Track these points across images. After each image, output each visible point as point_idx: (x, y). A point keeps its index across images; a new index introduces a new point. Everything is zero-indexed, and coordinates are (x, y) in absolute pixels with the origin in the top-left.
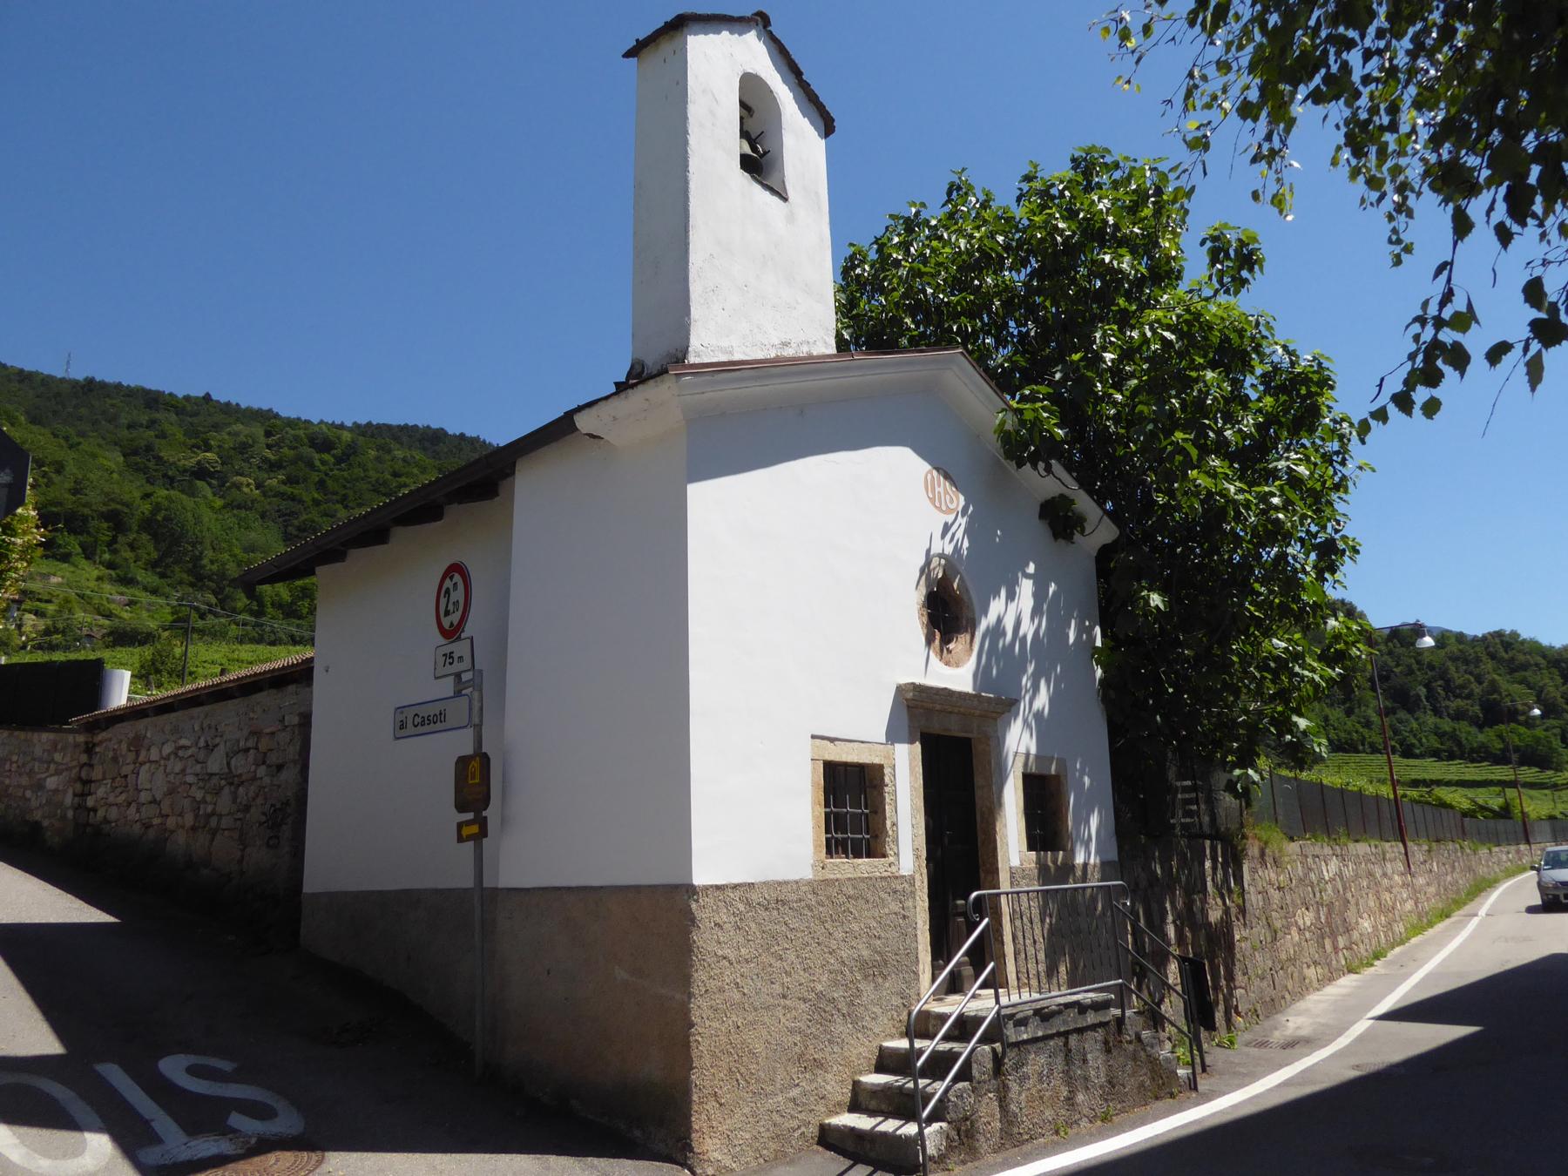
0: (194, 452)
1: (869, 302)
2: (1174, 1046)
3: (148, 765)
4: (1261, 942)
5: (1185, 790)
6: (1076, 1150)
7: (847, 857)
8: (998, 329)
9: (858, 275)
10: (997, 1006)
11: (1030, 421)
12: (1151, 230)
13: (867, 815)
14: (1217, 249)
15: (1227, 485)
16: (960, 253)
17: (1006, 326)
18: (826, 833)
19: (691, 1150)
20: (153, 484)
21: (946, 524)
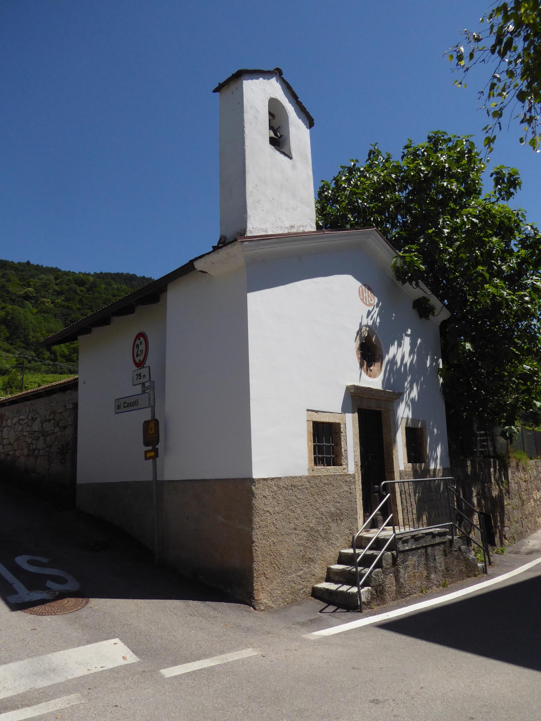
0: (23, 288)
1: (331, 208)
2: (476, 553)
3: (6, 428)
4: (517, 506)
5: (481, 435)
6: (431, 600)
7: (324, 466)
8: (392, 219)
9: (326, 195)
10: (394, 534)
11: (408, 261)
12: (466, 170)
13: (333, 446)
14: (499, 178)
15: (503, 292)
16: (374, 183)
17: (396, 218)
18: (314, 454)
19: (254, 599)
20: (5, 303)
21: (369, 311)
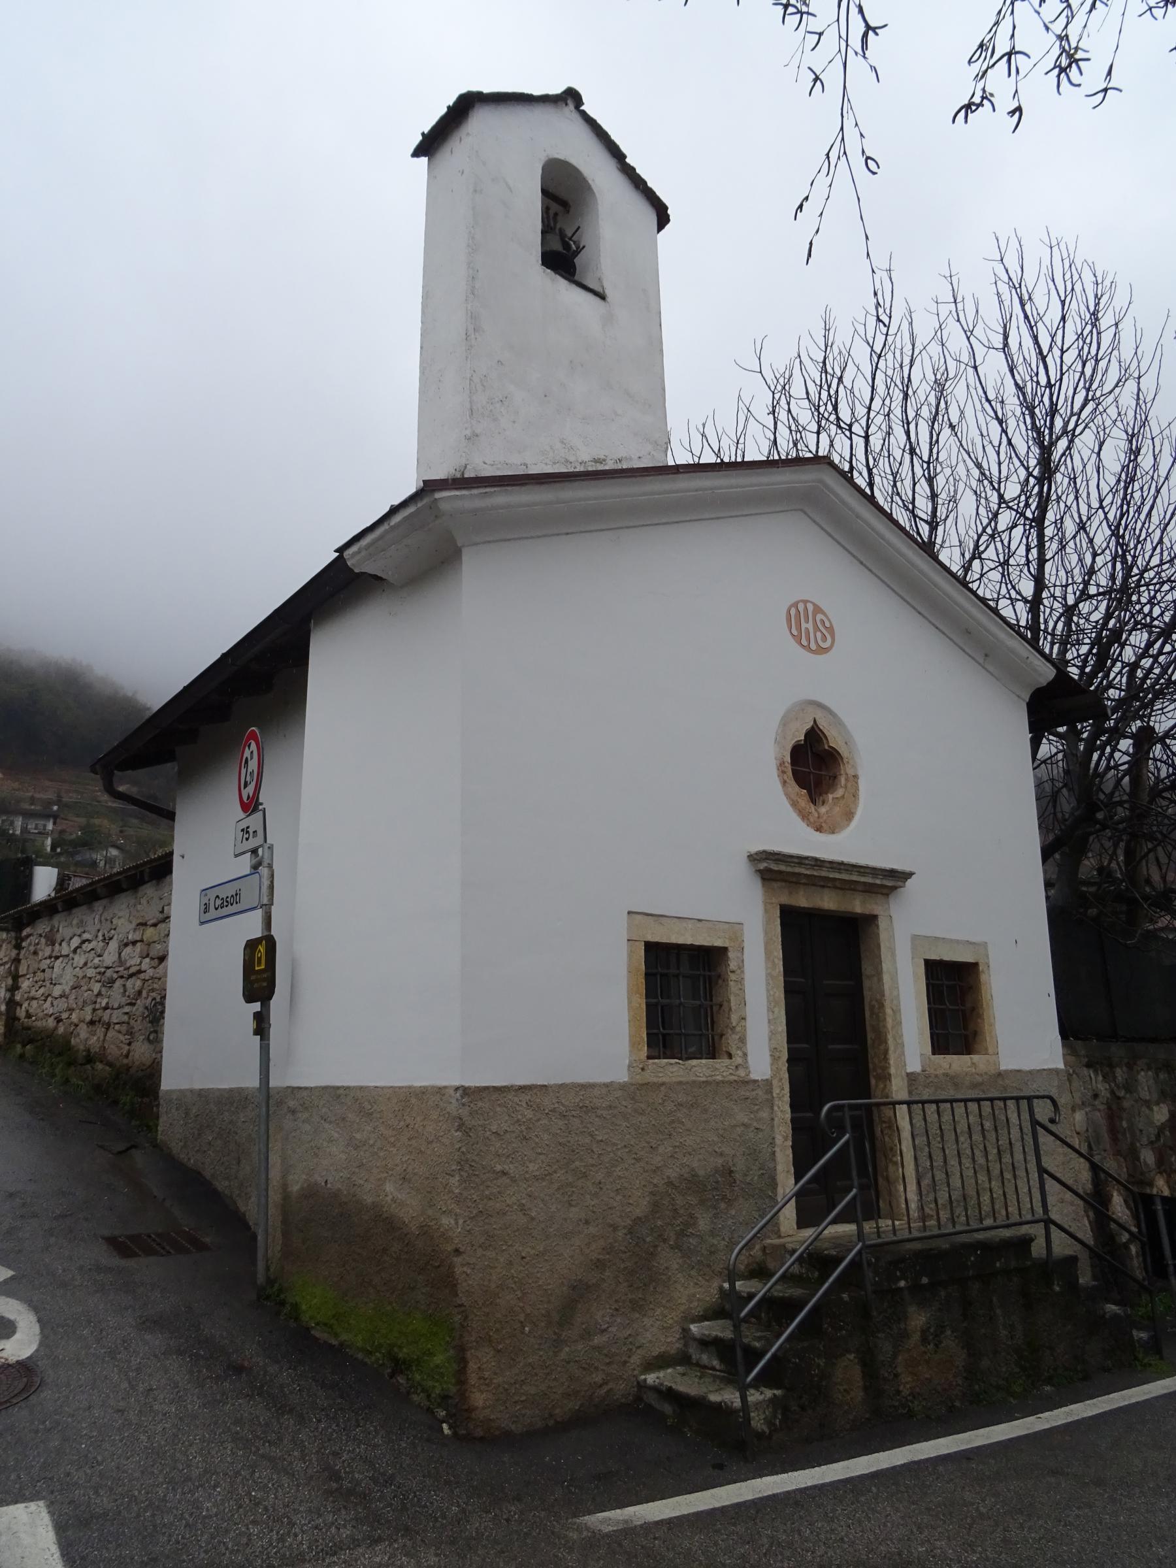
3: (61, 959)
10: (860, 1245)
